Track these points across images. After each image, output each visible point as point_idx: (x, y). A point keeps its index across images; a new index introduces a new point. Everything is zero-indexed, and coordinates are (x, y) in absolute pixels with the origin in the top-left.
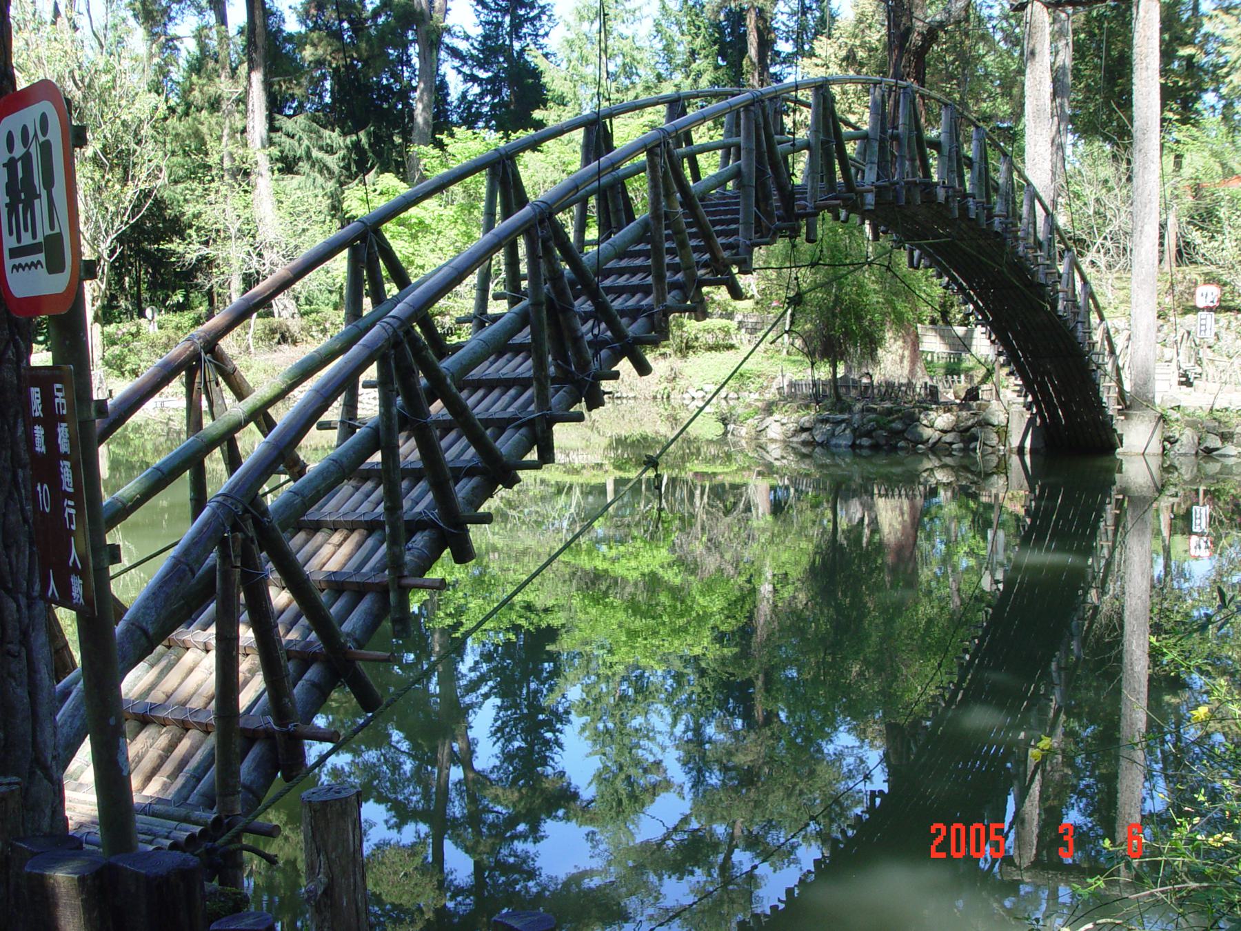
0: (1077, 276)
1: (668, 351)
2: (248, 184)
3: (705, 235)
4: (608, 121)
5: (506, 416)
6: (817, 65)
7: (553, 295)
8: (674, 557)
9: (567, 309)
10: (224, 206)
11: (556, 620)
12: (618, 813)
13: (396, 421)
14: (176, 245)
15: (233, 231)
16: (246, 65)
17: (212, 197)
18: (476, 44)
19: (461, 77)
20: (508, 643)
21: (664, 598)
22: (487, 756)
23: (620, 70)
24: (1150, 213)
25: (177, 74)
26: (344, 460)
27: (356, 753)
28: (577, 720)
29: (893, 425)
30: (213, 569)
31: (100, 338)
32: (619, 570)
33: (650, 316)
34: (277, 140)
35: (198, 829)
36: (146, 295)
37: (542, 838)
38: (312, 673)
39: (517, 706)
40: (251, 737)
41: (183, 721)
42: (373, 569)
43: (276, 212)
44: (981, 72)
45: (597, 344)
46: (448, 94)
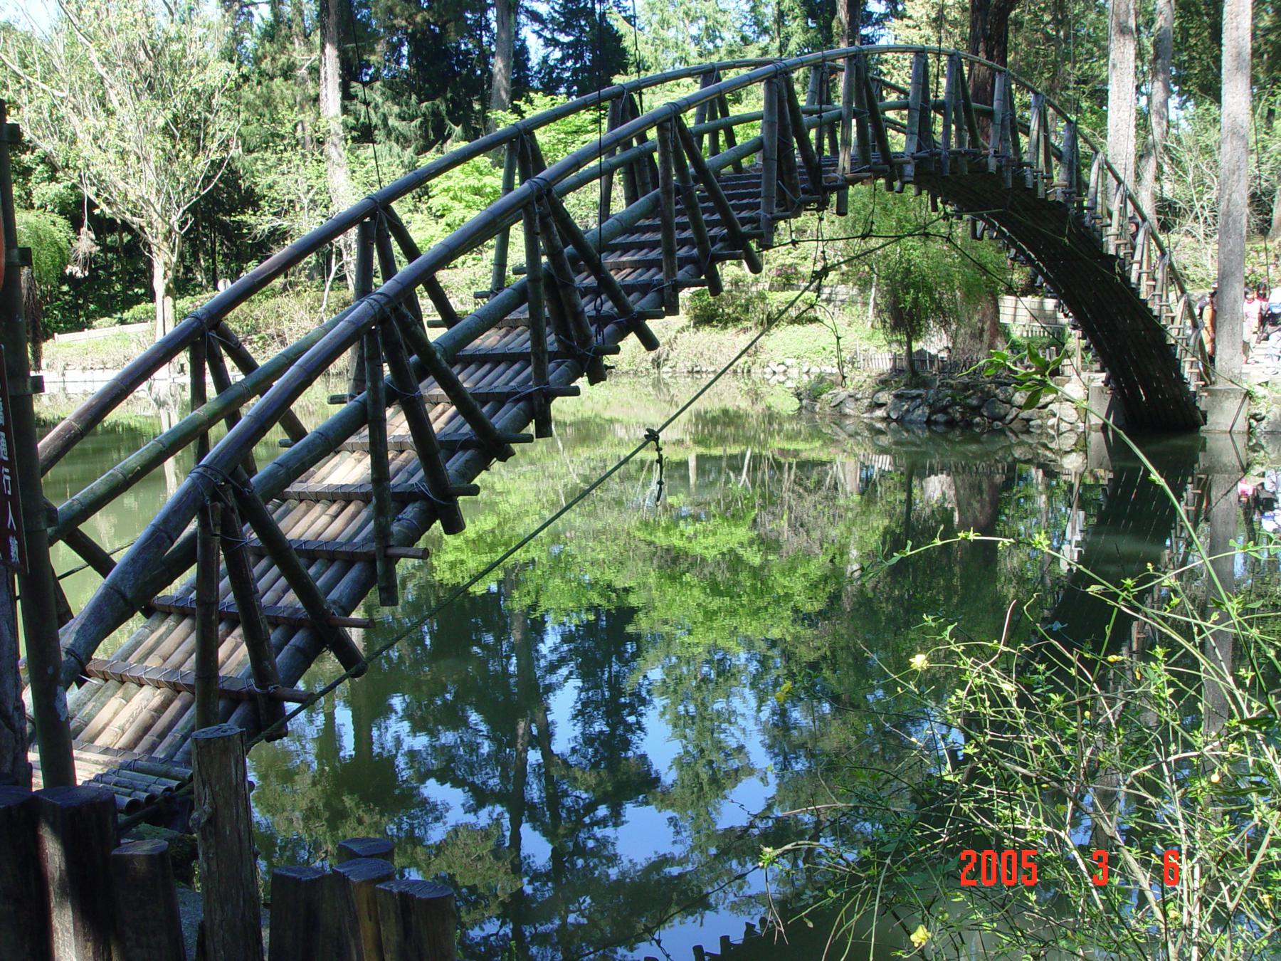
1: (748, 324)
2: (321, 154)
3: (721, 207)
4: (636, 97)
5: (506, 390)
6: (908, 27)
7: (553, 272)
8: (753, 534)
9: (568, 283)
10: (296, 176)
11: (633, 600)
12: (699, 798)
13: (383, 395)
14: (248, 218)
15: (306, 202)
16: (318, 32)
17: (284, 167)
18: (557, 7)
19: (541, 41)
20: (589, 626)
21: (744, 578)
22: (565, 736)
23: (703, 34)
24: (1239, 181)
25: (250, 43)
26: (330, 433)
27: (433, 734)
28: (659, 702)
29: (969, 401)
30: (193, 537)
31: (172, 311)
32: (697, 548)
33: (660, 291)
34: (352, 108)
35: (175, 783)
36: (221, 267)
37: (623, 823)
38: (297, 639)
39: (597, 686)
40: (235, 698)
41: (174, 684)
42: (364, 539)
45: (601, 320)
46: (528, 59)
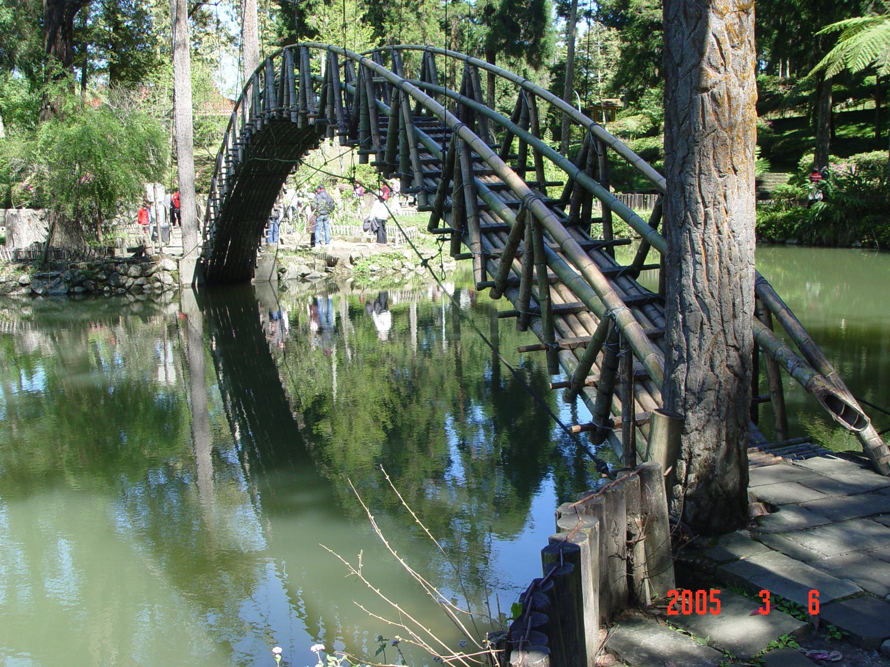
0: (240, 448)
43: (245, 43)
44: (688, 304)
